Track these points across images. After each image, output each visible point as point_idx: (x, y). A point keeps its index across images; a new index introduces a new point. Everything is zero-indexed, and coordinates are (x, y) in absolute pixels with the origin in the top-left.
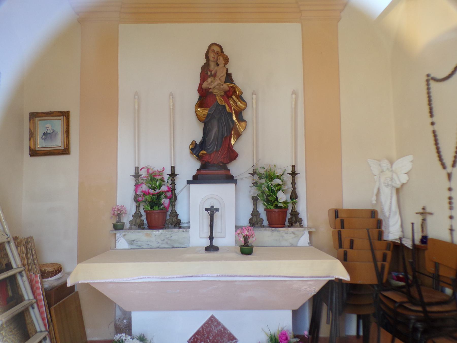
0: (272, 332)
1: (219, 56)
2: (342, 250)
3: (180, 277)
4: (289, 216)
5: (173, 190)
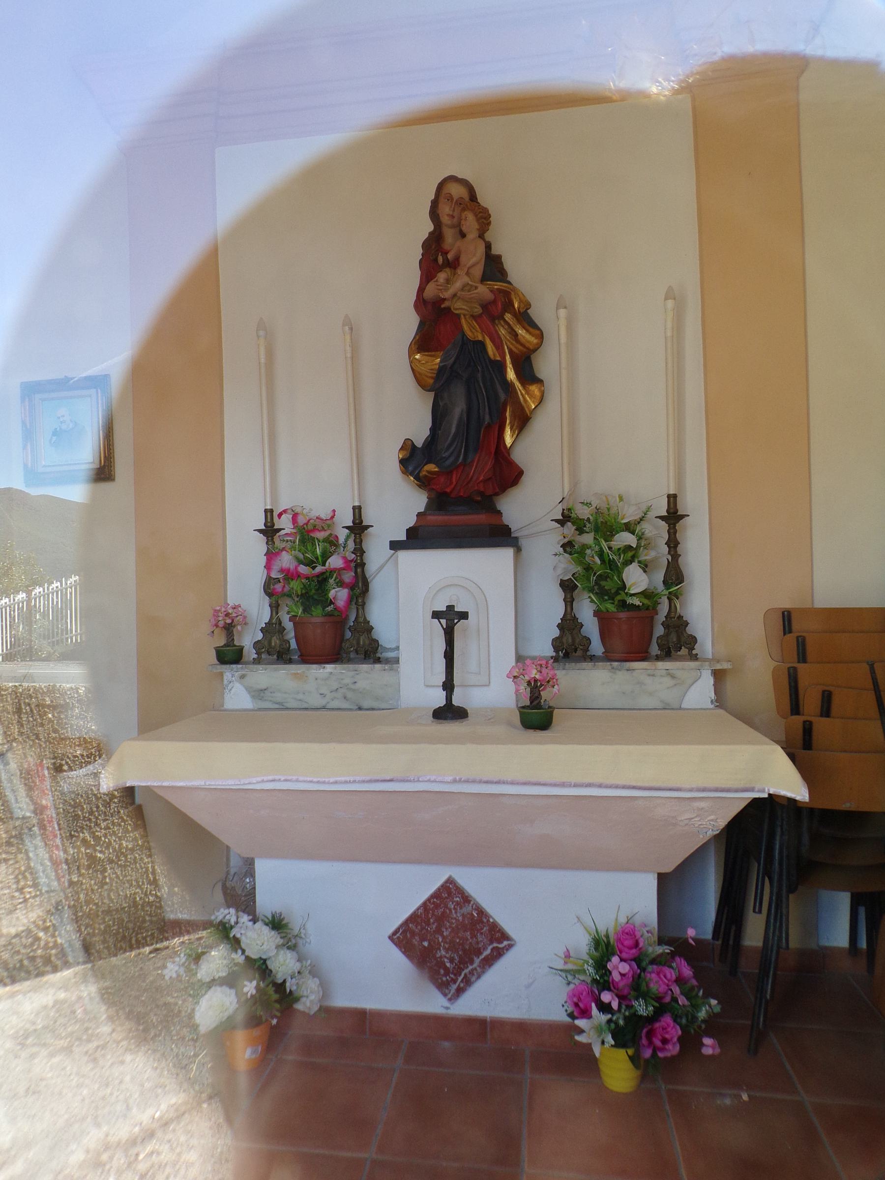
0: (602, 930)
1: (464, 210)
2: (798, 720)
3: (363, 782)
4: (659, 631)
5: (358, 564)
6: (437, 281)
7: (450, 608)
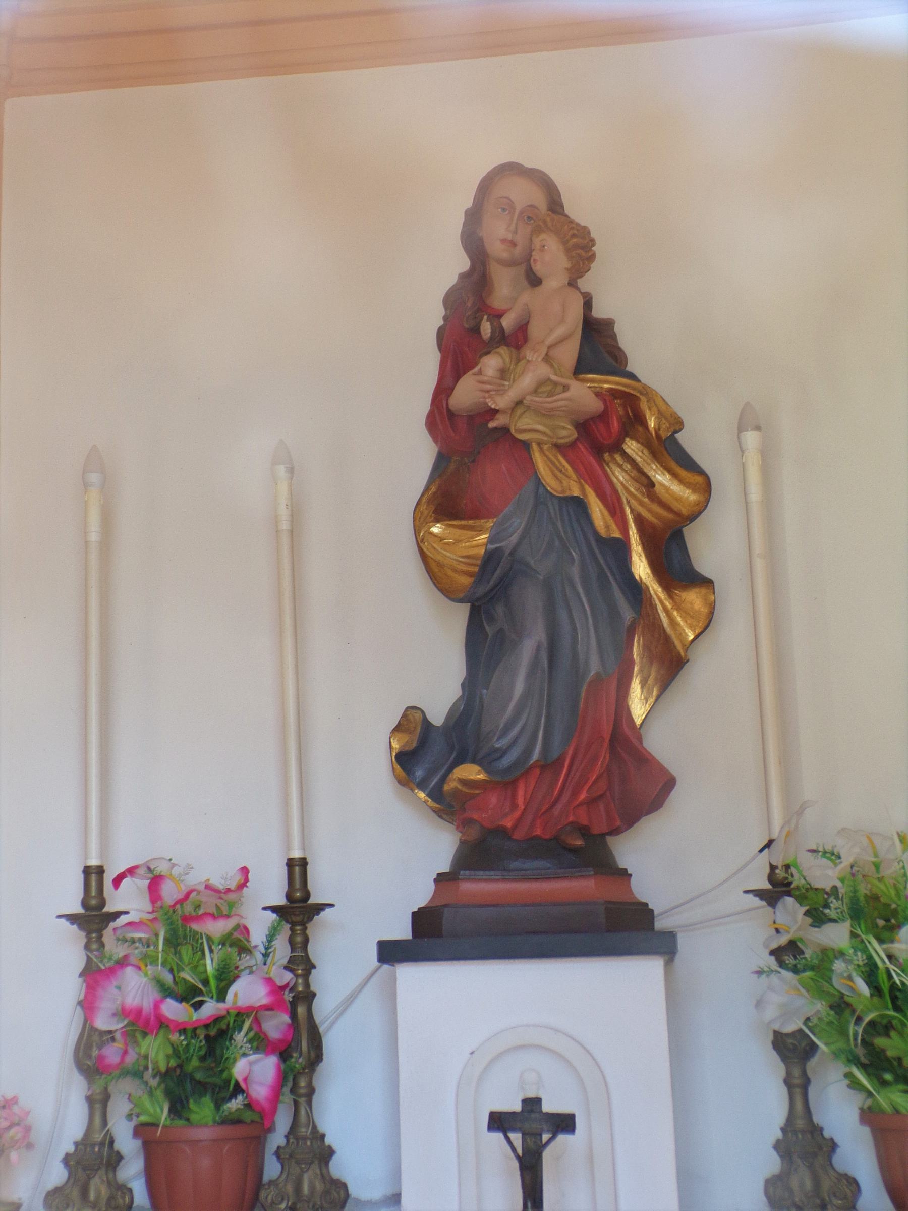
1: (537, 230)
5: (297, 998)
6: (480, 373)
7: (532, 1104)
